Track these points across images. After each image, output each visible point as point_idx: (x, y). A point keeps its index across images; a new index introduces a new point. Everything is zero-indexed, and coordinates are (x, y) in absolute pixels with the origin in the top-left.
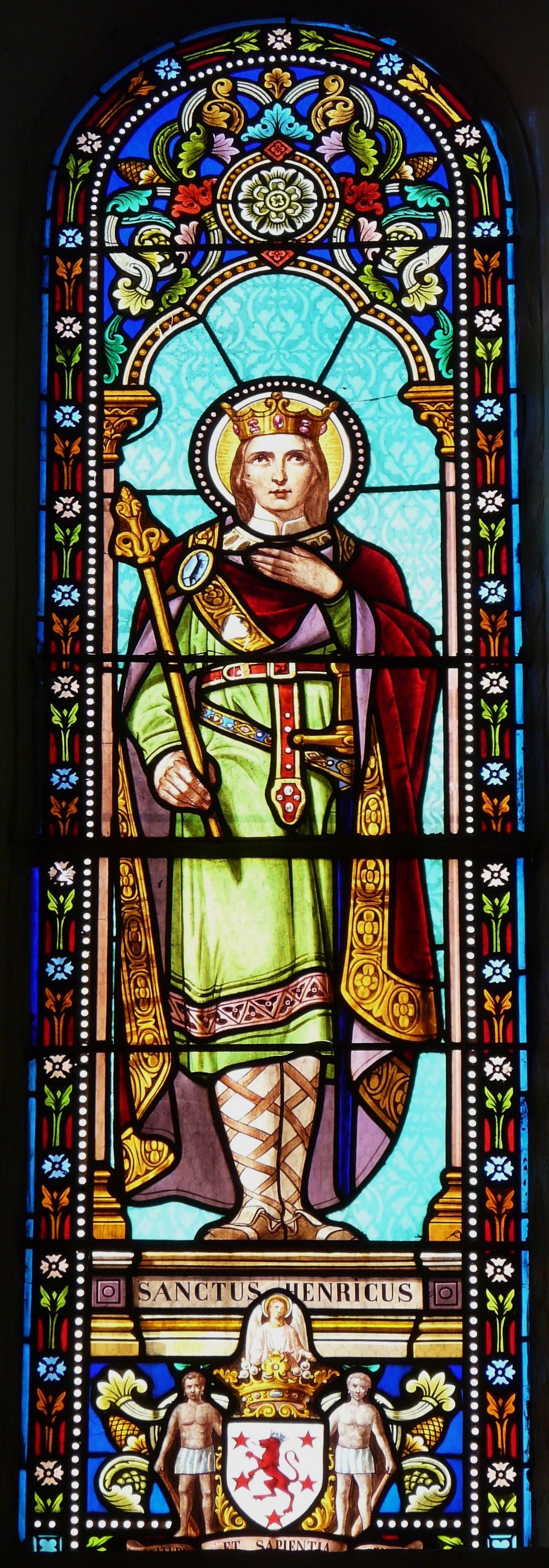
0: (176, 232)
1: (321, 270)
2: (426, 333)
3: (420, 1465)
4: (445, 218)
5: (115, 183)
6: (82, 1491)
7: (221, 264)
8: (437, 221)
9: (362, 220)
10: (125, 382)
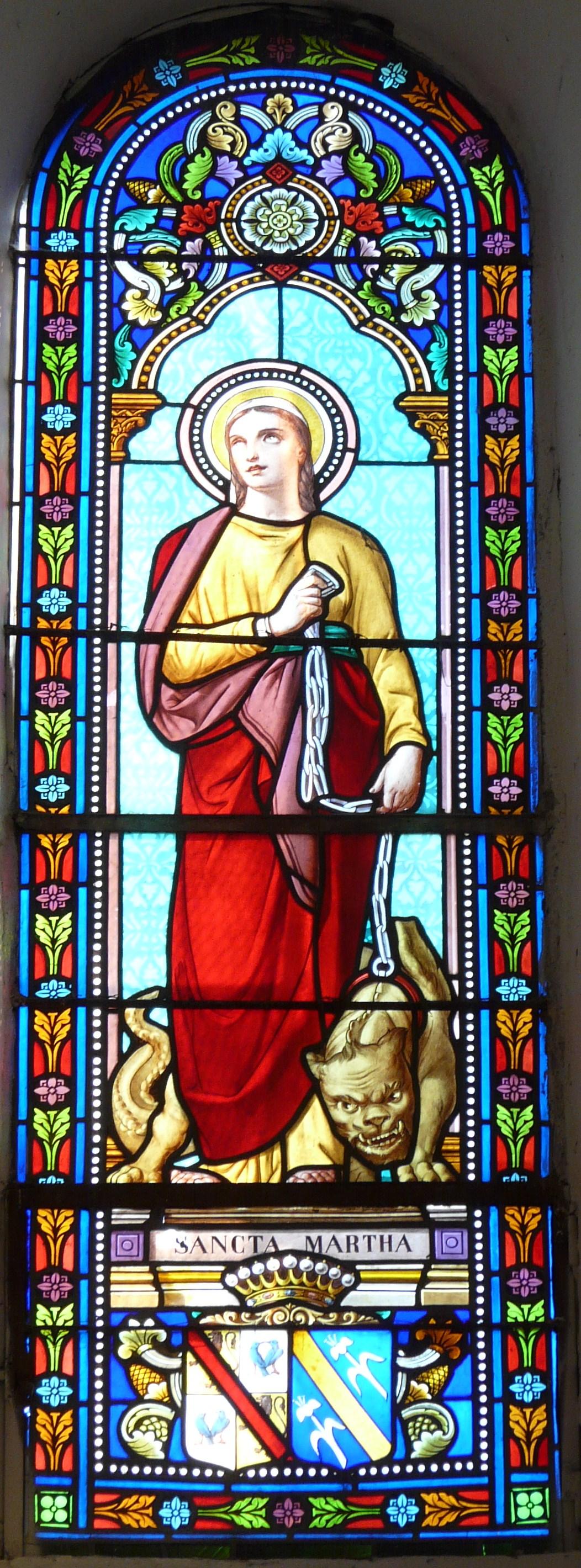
1: (323, 285)
2: (423, 346)
3: (422, 1411)
4: (441, 236)
6: (105, 1436)
7: (227, 278)
8: (433, 239)
9: (363, 239)
10: (134, 385)
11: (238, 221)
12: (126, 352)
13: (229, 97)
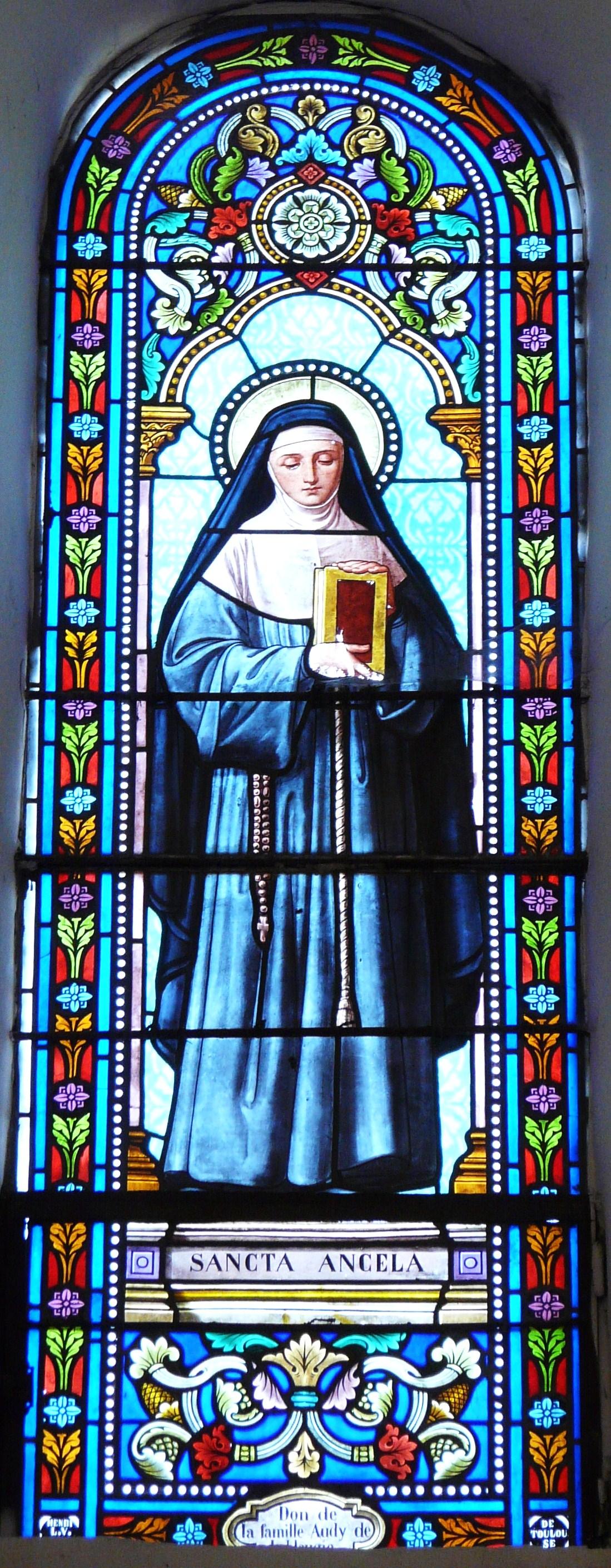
0: (212, 254)
1: (354, 293)
2: (453, 358)
4: (473, 246)
5: (154, 205)
7: (257, 285)
8: (465, 250)
9: (393, 247)
10: (163, 399)
11: (269, 222)
12: (153, 366)
13: (260, 100)
